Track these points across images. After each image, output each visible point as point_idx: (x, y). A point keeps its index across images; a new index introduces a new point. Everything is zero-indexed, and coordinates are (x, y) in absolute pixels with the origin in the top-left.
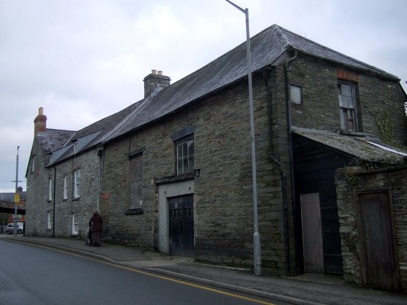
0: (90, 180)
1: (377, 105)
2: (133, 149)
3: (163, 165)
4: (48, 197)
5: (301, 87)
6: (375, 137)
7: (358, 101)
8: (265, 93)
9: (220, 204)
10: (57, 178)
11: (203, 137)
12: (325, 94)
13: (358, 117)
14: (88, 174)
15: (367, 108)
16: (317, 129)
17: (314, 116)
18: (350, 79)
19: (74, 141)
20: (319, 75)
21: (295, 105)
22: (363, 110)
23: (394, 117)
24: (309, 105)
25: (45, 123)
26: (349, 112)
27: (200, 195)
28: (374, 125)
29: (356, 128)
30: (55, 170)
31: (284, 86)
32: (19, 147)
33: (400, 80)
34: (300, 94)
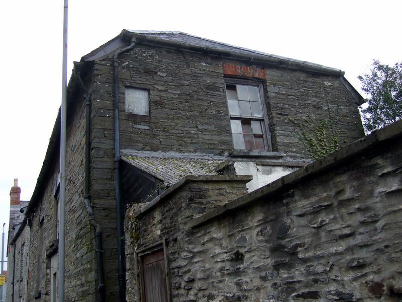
1: (306, 110)
5: (148, 90)
6: (303, 158)
7: (268, 106)
12: (199, 99)
13: (270, 129)
15: (287, 115)
16: (181, 152)
17: (173, 131)
18: (251, 75)
20: (187, 71)
21: (134, 117)
22: (277, 118)
23: (340, 126)
24: (165, 116)
25: (19, 195)
28: (300, 139)
29: (269, 147)
31: (110, 90)
32: (5, 224)
33: (344, 73)
34: (147, 101)
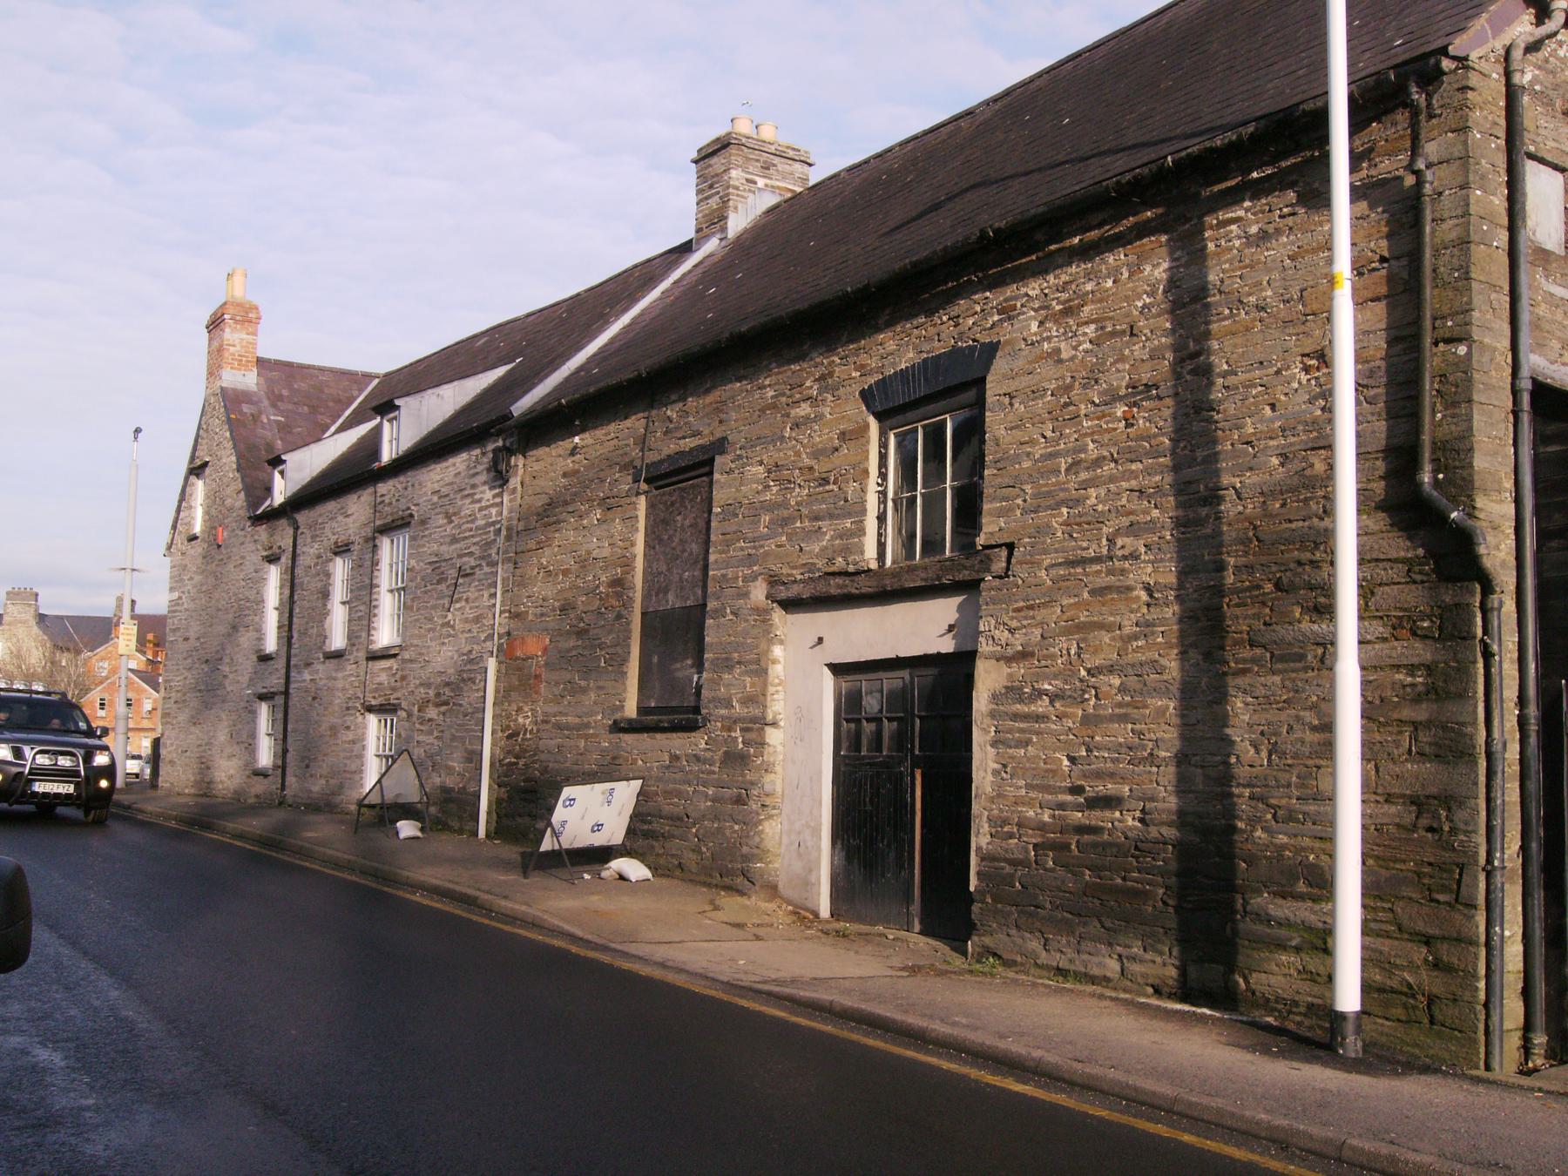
0: (453, 573)
2: (667, 448)
3: (817, 518)
4: (261, 639)
8: (693, 870)
9: (1120, 705)
10: (301, 560)
11: (1037, 393)
14: (444, 548)
19: (385, 408)
21: (1543, 255)
26: (1385, 619)
27: (1009, 660)
30: (297, 528)
